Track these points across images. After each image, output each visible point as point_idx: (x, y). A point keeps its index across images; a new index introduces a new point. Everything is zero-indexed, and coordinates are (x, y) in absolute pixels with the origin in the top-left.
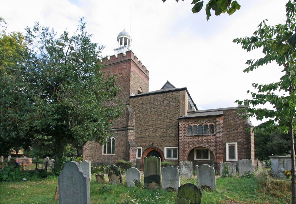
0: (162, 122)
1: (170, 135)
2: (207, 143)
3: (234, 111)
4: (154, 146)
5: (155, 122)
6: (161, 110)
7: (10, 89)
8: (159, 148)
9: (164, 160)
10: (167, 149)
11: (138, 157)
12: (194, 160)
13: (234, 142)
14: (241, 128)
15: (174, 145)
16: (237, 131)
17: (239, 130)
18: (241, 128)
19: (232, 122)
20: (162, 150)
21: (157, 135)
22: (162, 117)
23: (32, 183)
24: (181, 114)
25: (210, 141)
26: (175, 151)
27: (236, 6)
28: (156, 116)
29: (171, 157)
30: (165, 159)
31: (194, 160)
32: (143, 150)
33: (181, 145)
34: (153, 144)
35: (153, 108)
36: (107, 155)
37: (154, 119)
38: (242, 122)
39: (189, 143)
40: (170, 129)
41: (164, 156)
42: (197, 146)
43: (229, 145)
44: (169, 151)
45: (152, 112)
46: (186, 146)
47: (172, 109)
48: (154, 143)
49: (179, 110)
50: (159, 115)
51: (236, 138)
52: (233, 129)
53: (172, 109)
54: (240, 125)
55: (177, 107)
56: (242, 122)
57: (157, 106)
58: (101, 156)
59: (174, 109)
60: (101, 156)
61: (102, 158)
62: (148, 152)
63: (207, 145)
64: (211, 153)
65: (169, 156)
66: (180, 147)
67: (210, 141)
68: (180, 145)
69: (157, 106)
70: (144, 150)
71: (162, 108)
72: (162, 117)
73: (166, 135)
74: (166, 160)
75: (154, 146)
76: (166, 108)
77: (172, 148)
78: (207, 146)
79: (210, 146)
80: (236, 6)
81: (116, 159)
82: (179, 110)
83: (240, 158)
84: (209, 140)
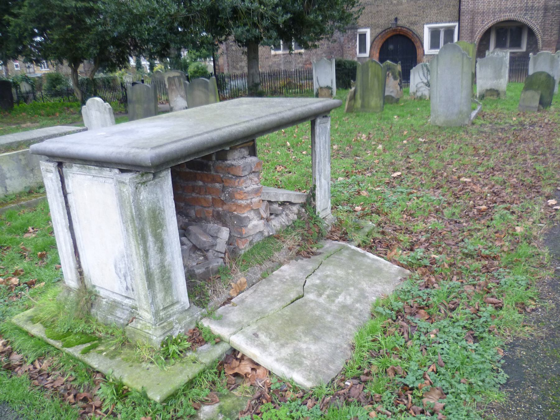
4: (399, 23)
7: (10, 279)
8: (412, 27)
9: (424, 54)
11: (360, 52)
15: (448, 19)
20: (418, 32)
23: (43, 336)
25: (533, 6)
26: (449, 32)
32: (371, 34)
33: (466, 19)
34: (396, 19)
36: (284, 54)
41: (423, 46)
42: (502, 19)
43: (512, 55)
44: (435, 34)
46: (479, 18)
48: (399, 17)
58: (267, 58)
60: (267, 58)
61: (270, 63)
62: (385, 39)
63: (525, 14)
64: (531, 33)
65: (434, 44)
66: (462, 24)
68: (462, 18)
70: (375, 35)
74: (427, 55)
75: (399, 23)
77: (442, 27)
78: (525, 19)
79: (531, 17)
81: (306, 61)
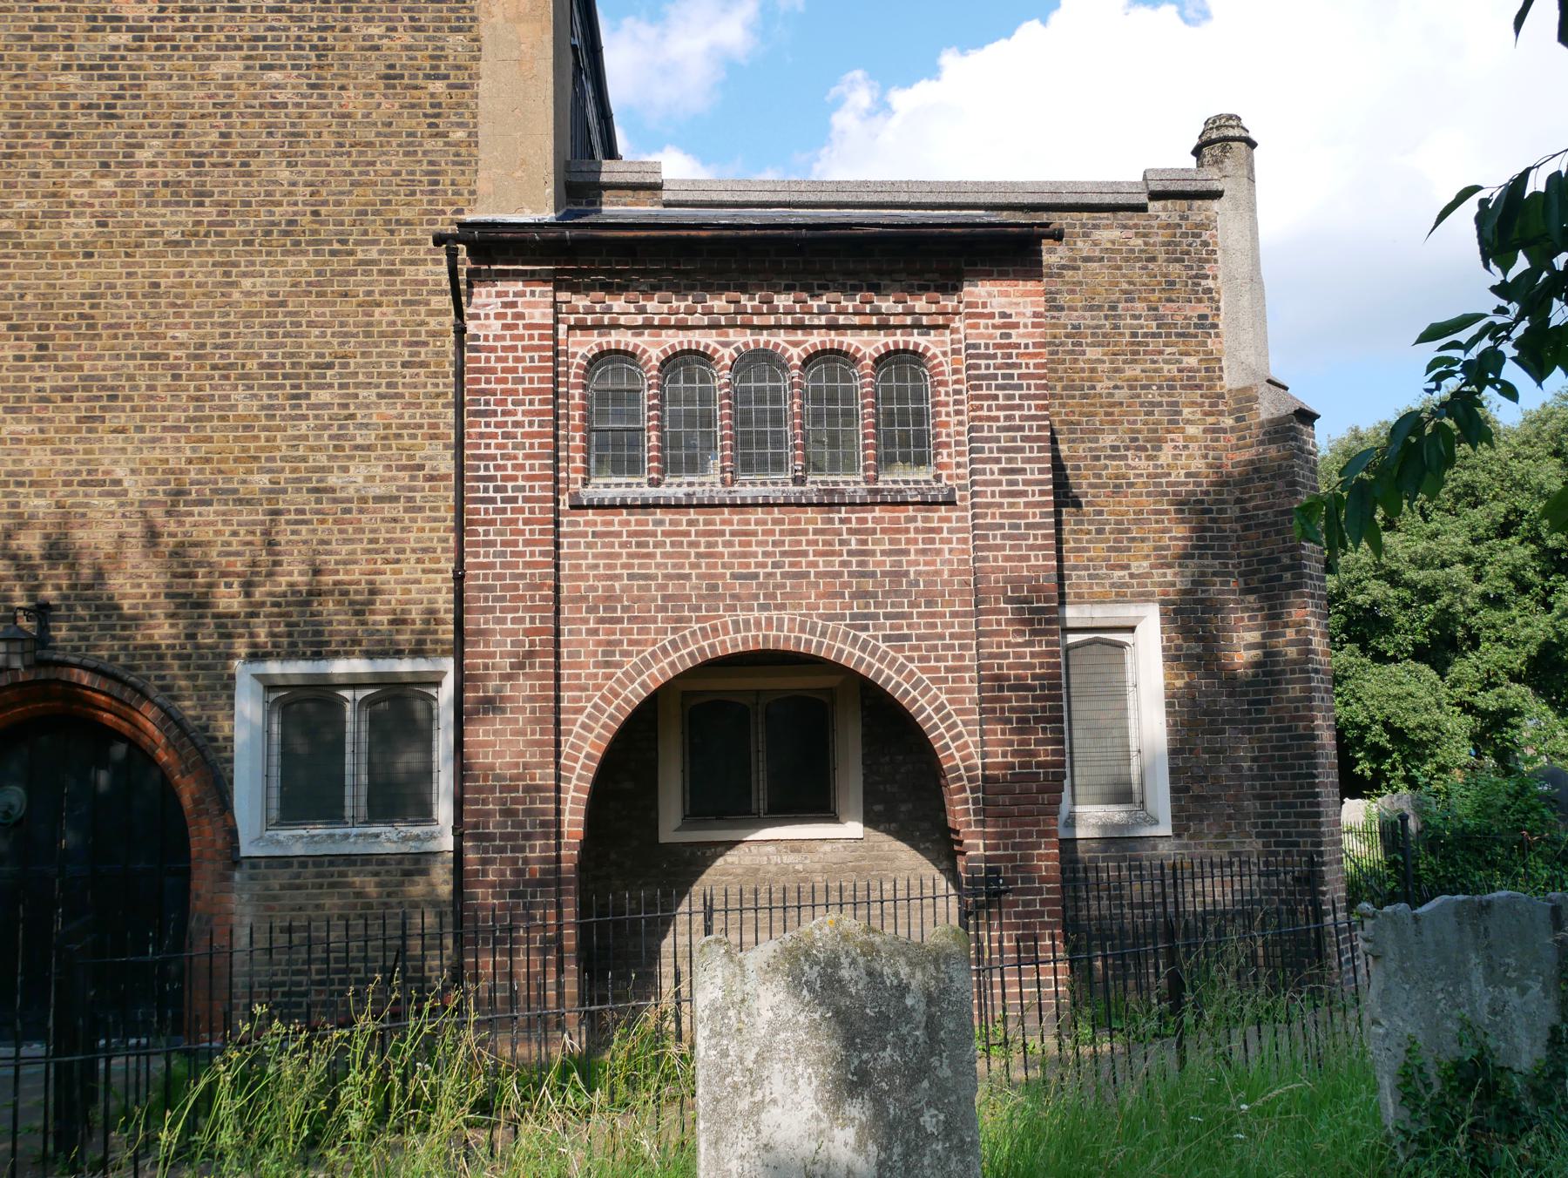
0: (200, 270)
1: (333, 480)
2: (862, 594)
3: (1116, 234)
5: (84, 279)
6: (196, 94)
9: (235, 860)
10: (270, 685)
12: (663, 839)
13: (1120, 596)
14: (1191, 430)
16: (1141, 464)
17: (1165, 456)
18: (1191, 430)
19: (1093, 353)
21: (120, 472)
22: (210, 212)
24: (482, 186)
25: (897, 575)
27: (1206, 15)
28: (108, 184)
29: (331, 812)
30: (248, 848)
31: (663, 839)
35: (58, 57)
37: (80, 226)
38: (1192, 361)
39: (610, 599)
40: (323, 396)
45: (51, 118)
47: (353, 100)
49: (460, 134)
50: (164, 173)
51: (1147, 547)
52: (1108, 440)
53: (353, 100)
54: (1182, 396)
55: (439, 86)
56: (1192, 361)
57: (125, 38)
59: (389, 106)
67: (897, 575)
69: (125, 38)
71: (204, 81)
72: (210, 212)
73: (263, 480)
74: (254, 861)
76: (276, 76)
80: (1206, 15)
82: (460, 134)
83: (1196, 789)
84: (880, 563)
